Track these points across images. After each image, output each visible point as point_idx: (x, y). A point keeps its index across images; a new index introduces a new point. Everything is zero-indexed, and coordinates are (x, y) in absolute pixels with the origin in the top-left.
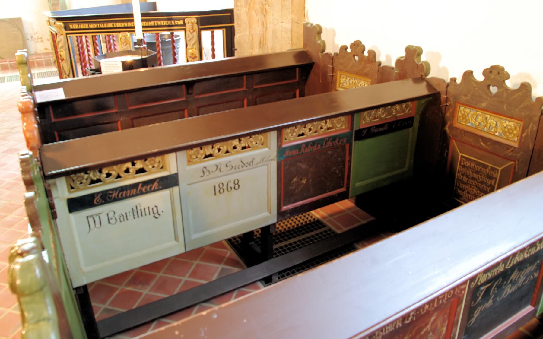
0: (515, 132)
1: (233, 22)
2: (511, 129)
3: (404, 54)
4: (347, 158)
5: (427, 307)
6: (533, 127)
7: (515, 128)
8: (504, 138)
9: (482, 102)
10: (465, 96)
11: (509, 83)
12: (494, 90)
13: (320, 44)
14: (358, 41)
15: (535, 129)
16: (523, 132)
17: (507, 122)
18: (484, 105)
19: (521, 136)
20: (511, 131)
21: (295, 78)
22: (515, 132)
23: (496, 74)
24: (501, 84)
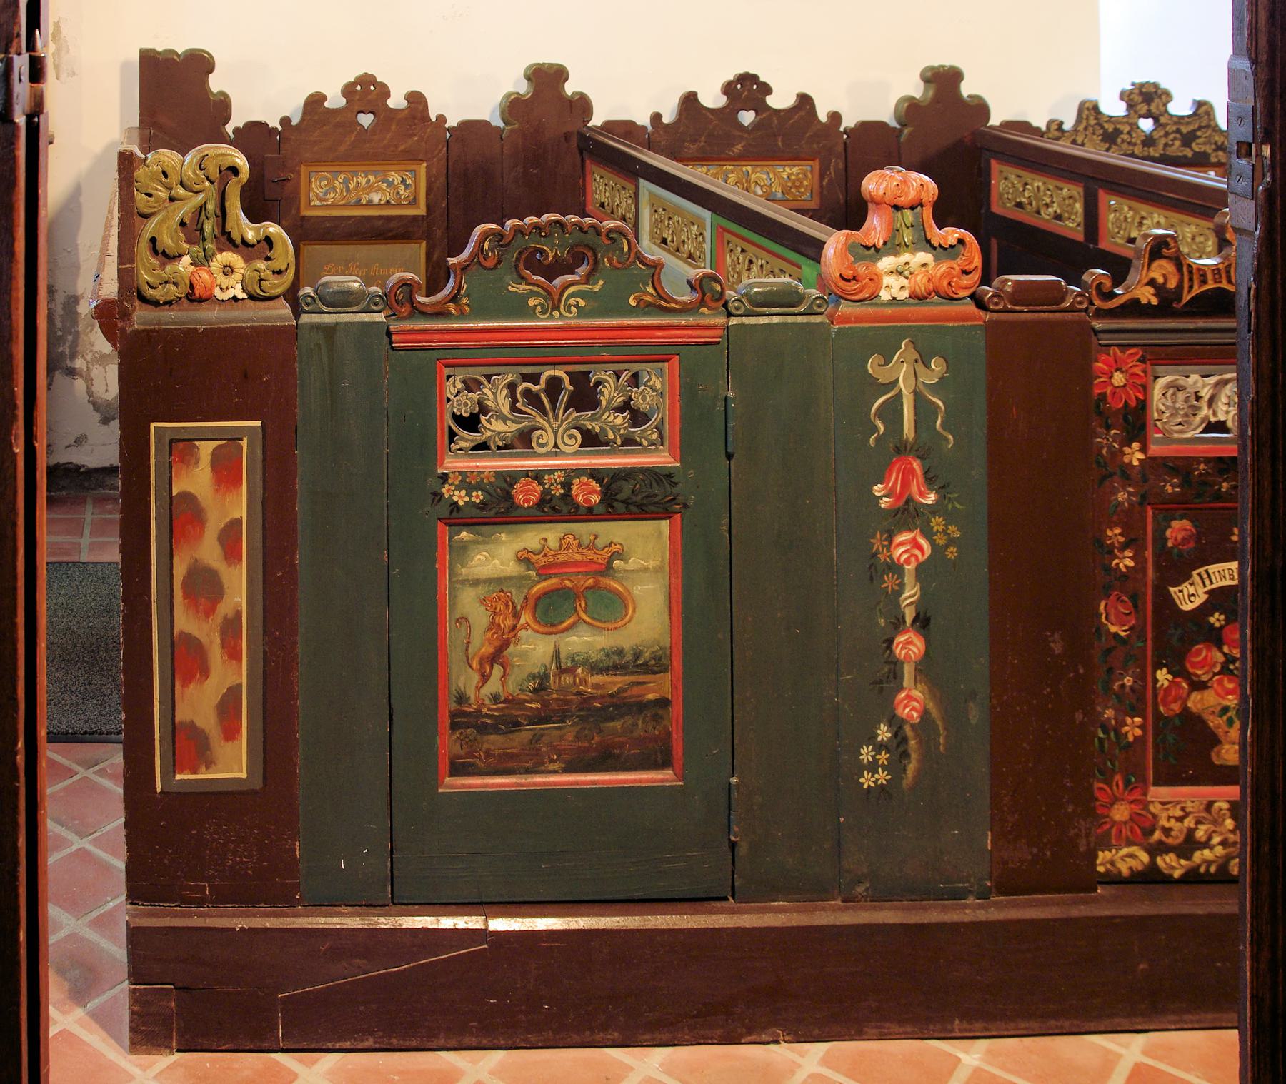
0: (805, 183)
1: (132, 261)
2: (798, 180)
3: (523, 88)
4: (354, 309)
5: (333, 271)
6: (837, 164)
7: (805, 175)
8: (629, 242)
9: (734, 145)
10: (694, 141)
11: (774, 101)
12: (747, 117)
13: (952, 1023)
14: (366, 80)
15: (841, 165)
16: (822, 177)
17: (788, 169)
18: (738, 148)
19: (821, 186)
20: (798, 184)
21: (938, 407)
22: (805, 183)
23: (747, 89)
24: (760, 106)
